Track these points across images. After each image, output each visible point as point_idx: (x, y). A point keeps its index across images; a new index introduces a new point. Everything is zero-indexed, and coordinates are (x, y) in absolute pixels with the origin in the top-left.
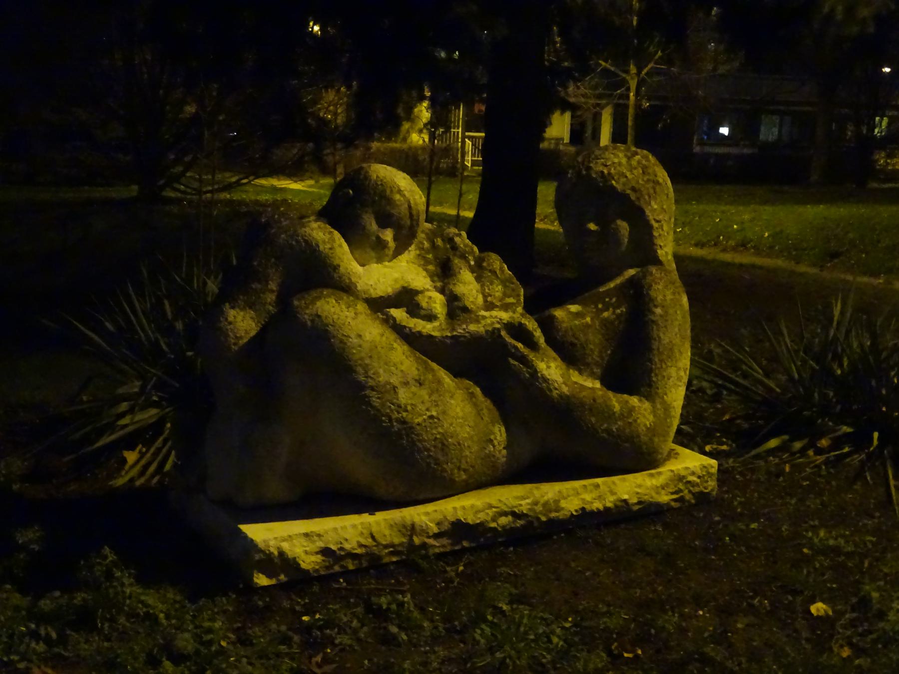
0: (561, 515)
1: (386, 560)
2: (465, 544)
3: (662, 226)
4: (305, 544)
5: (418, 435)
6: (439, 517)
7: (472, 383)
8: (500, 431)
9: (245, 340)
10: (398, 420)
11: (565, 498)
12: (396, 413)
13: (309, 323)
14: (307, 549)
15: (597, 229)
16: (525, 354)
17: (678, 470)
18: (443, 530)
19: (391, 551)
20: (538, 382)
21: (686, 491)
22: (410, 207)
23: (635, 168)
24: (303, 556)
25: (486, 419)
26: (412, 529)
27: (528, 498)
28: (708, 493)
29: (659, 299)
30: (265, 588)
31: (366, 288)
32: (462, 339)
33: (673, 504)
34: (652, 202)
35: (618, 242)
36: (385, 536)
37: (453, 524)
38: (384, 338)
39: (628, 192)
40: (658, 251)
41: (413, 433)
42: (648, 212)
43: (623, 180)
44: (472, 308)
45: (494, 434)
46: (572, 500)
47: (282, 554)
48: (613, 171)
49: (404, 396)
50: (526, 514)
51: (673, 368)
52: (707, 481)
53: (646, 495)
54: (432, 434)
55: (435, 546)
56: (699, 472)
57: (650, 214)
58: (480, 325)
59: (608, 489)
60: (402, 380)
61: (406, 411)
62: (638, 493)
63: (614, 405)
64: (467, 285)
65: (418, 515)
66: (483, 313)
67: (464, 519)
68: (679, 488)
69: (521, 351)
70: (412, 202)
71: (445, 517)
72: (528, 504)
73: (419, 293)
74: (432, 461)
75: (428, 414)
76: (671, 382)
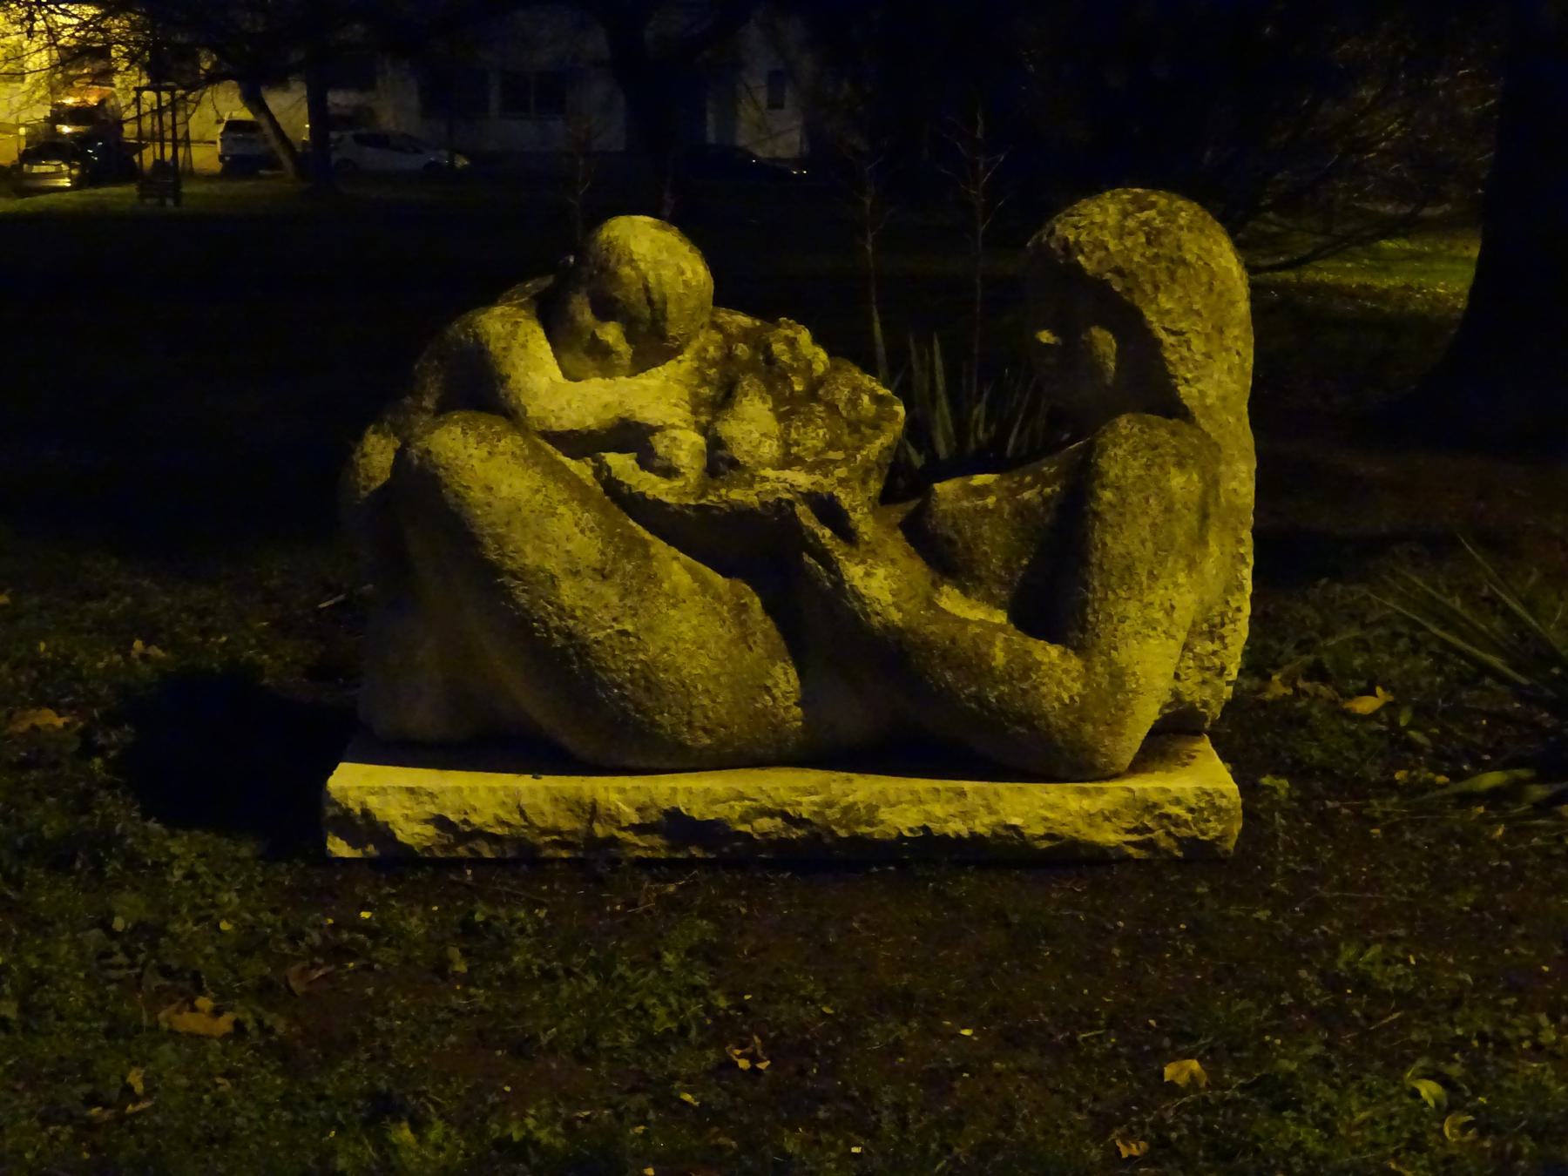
0: (876, 832)
2: (696, 852)
3: (1188, 343)
4: (408, 804)
5: (598, 659)
6: (642, 798)
7: (748, 588)
9: (379, 484)
10: (558, 630)
12: (555, 618)
13: (416, 462)
14: (409, 812)
15: (1056, 343)
16: (829, 547)
17: (1144, 790)
18: (648, 822)
20: (846, 598)
21: (1160, 832)
22: (647, 289)
23: (1131, 234)
24: (401, 822)
25: (759, 651)
26: (592, 811)
27: (816, 793)
28: (1211, 844)
29: (1112, 474)
30: (344, 861)
31: (542, 414)
32: (716, 512)
33: (1131, 850)
34: (1160, 296)
35: (1097, 368)
36: (543, 814)
37: (666, 813)
38: (539, 497)
39: (1108, 276)
40: (1179, 388)
41: (588, 654)
42: (1150, 316)
43: (1100, 254)
45: (772, 677)
46: (906, 810)
47: (366, 813)
48: (1083, 238)
49: (568, 593)
53: (1064, 824)
54: (626, 662)
55: (636, 846)
56: (1193, 802)
57: (1153, 319)
58: (750, 492)
61: (574, 617)
62: (1045, 819)
63: (995, 655)
64: (745, 422)
65: (606, 789)
66: (769, 472)
67: (687, 810)
68: (1142, 823)
69: (823, 541)
70: (652, 280)
71: (652, 800)
74: (630, 706)
75: (617, 627)
76: (1127, 627)
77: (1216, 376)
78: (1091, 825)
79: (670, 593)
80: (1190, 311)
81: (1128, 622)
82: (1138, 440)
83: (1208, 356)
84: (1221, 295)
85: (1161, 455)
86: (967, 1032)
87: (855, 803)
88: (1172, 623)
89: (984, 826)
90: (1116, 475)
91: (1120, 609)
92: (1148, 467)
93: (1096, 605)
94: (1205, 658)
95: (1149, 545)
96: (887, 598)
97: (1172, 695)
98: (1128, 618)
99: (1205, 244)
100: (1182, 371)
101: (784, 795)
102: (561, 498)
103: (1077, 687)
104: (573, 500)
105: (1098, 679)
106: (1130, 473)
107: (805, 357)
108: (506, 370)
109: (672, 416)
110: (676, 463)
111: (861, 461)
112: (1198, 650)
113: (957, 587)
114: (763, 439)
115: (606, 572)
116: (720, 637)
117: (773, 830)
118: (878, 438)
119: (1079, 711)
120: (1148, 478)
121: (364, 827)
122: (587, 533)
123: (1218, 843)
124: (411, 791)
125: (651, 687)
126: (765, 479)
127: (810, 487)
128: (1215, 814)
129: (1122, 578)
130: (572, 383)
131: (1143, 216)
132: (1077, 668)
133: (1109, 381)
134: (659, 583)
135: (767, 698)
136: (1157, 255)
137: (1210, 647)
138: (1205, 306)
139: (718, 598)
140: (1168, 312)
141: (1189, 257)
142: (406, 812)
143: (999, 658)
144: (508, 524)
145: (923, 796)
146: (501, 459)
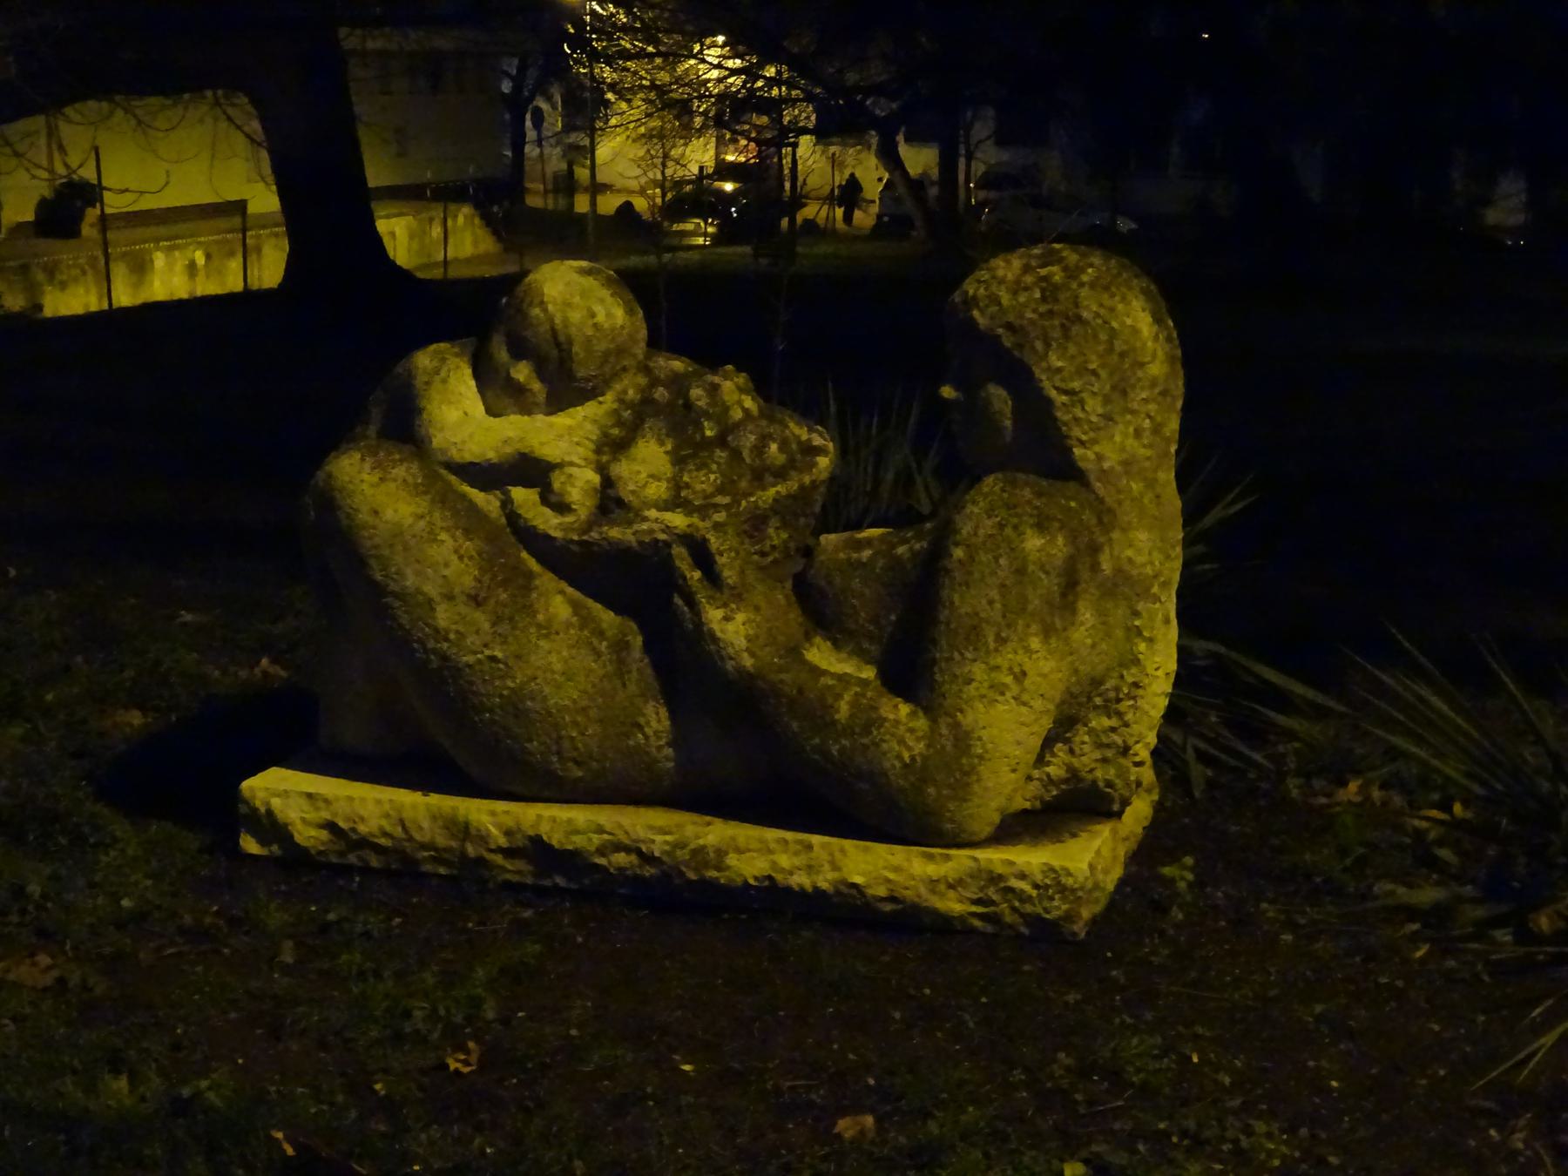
1: (428, 868)
2: (560, 881)
3: (1082, 403)
6: (509, 822)
8: (657, 714)
10: (434, 651)
11: (739, 851)
17: (990, 861)
19: (432, 855)
22: (554, 332)
23: (1026, 289)
25: (632, 688)
26: (464, 831)
28: (1054, 924)
29: (964, 532)
32: (596, 548)
33: (977, 923)
34: (1050, 353)
36: (421, 828)
37: (530, 838)
38: (422, 523)
39: (1000, 331)
40: (1075, 450)
44: (630, 501)
45: (644, 715)
46: (753, 858)
47: (270, 813)
50: (659, 858)
51: (978, 663)
52: (1052, 899)
53: (907, 888)
56: (1039, 878)
57: (1044, 377)
58: (628, 531)
59: (829, 858)
60: (444, 591)
61: (447, 640)
62: (888, 881)
68: (986, 894)
70: (557, 321)
71: (518, 824)
72: (666, 842)
73: (556, 468)
75: (487, 652)
76: (971, 690)
77: (1118, 438)
78: (933, 891)
79: (543, 623)
80: (1082, 371)
81: (974, 684)
82: (996, 498)
83: (1108, 418)
84: (1123, 355)
85: (1017, 515)
86: (687, 1068)
87: (704, 847)
88: (1023, 690)
89: (826, 881)
90: (968, 533)
91: (966, 670)
92: (1001, 526)
93: (943, 665)
94: (1101, 734)
95: (998, 606)
96: (742, 643)
97: (1067, 771)
98: (973, 680)
99: (1107, 302)
100: (1076, 432)
101: (642, 833)
102: (444, 524)
103: (920, 747)
104: (457, 528)
105: (943, 741)
106: (981, 532)
107: (724, 403)
108: (423, 403)
109: (569, 454)
110: (568, 499)
111: (745, 508)
112: (1093, 724)
113: (829, 639)
114: (651, 480)
115: (480, 599)
116: (591, 671)
117: (628, 866)
118: (774, 486)
119: (920, 772)
120: (1000, 538)
121: (271, 828)
122: (466, 560)
123: (1061, 923)
124: (310, 796)
125: (519, 713)
126: (645, 519)
127: (686, 528)
128: (1059, 892)
129: (967, 638)
130: (491, 418)
131: (1043, 272)
132: (923, 727)
133: (1008, 439)
134: (534, 613)
135: (640, 736)
136: (1051, 313)
137: (1106, 722)
138: (1103, 366)
139: (601, 634)
140: (1059, 370)
141: (1085, 314)
142: (304, 815)
143: (843, 710)
144: (391, 546)
145: (773, 846)
146: (392, 485)
